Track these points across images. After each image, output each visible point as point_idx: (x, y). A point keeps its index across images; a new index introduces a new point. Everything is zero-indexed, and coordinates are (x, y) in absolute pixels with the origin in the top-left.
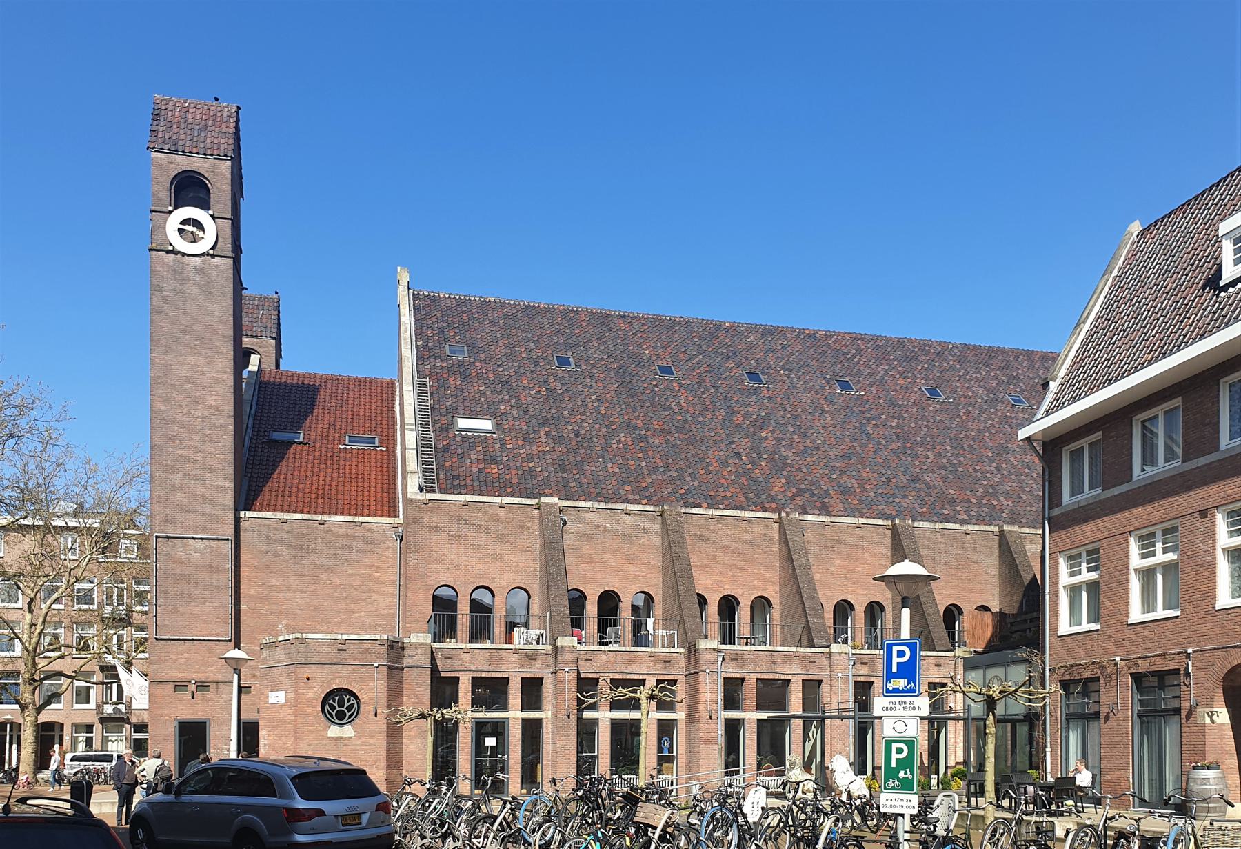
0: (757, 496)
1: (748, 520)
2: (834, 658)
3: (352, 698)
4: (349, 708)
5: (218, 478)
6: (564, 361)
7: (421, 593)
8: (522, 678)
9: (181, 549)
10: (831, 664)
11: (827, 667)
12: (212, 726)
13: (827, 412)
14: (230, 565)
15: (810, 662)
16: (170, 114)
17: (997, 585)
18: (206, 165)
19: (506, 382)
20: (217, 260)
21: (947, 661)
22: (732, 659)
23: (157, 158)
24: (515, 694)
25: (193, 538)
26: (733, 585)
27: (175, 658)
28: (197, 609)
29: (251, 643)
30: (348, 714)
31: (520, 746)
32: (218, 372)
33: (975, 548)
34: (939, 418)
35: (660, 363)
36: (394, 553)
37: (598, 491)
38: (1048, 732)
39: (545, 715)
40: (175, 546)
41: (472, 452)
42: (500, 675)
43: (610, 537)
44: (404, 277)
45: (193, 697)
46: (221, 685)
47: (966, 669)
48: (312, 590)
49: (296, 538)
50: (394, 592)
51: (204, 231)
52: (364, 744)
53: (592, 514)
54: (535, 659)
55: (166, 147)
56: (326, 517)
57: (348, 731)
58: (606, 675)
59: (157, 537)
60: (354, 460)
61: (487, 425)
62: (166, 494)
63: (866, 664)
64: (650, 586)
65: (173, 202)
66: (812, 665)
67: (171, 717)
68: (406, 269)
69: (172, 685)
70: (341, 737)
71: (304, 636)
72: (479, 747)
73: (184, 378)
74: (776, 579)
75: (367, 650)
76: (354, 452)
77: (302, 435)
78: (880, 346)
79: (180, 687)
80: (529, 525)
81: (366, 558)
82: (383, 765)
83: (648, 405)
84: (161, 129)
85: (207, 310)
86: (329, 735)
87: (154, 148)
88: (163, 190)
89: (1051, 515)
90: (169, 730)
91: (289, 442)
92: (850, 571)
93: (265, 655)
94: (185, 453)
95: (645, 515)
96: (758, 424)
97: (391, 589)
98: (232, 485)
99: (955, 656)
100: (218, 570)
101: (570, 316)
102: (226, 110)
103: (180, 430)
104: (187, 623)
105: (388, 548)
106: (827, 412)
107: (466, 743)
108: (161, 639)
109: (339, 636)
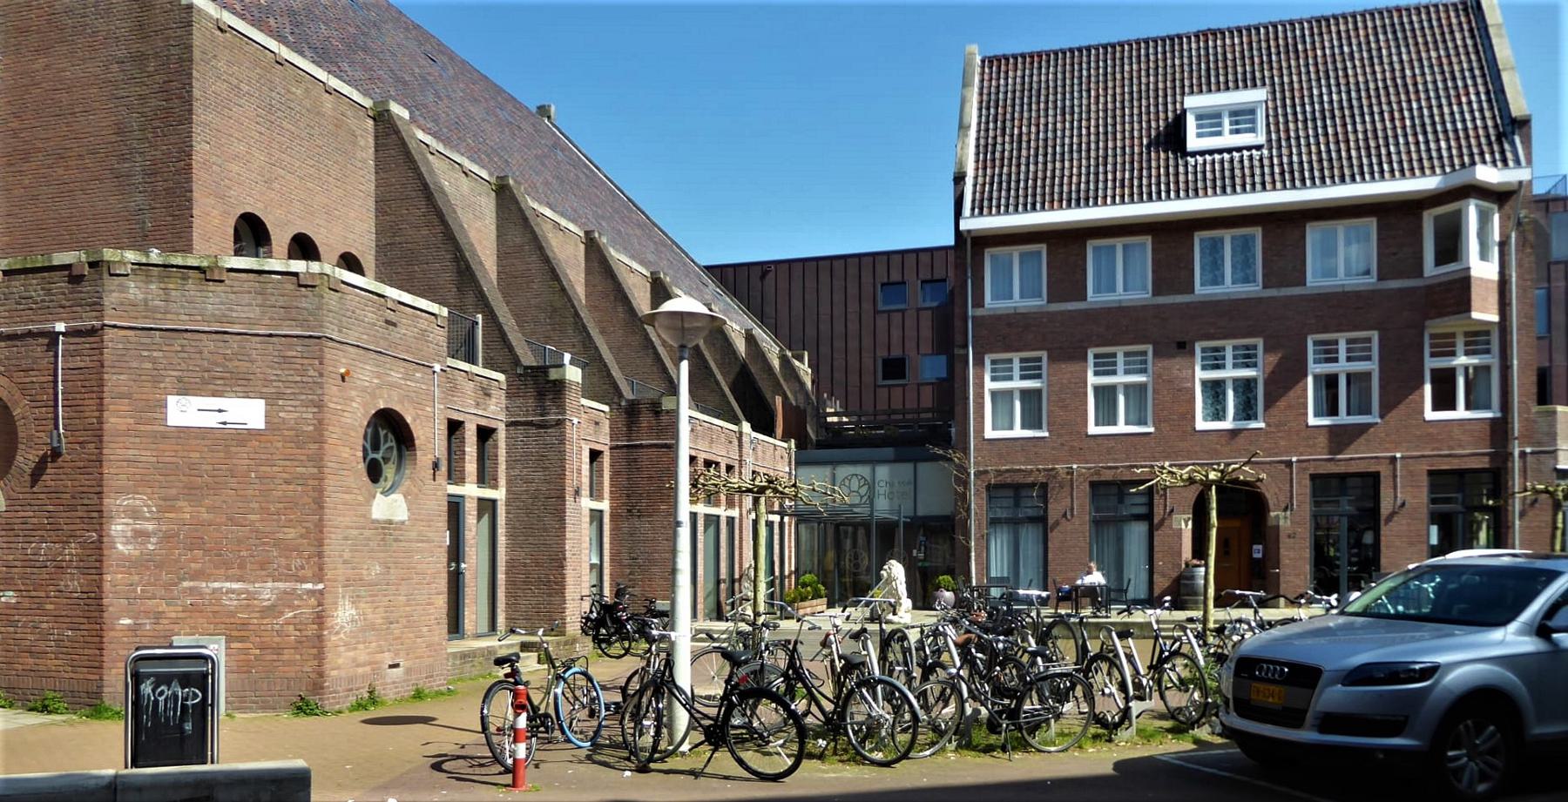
70: (390, 522)
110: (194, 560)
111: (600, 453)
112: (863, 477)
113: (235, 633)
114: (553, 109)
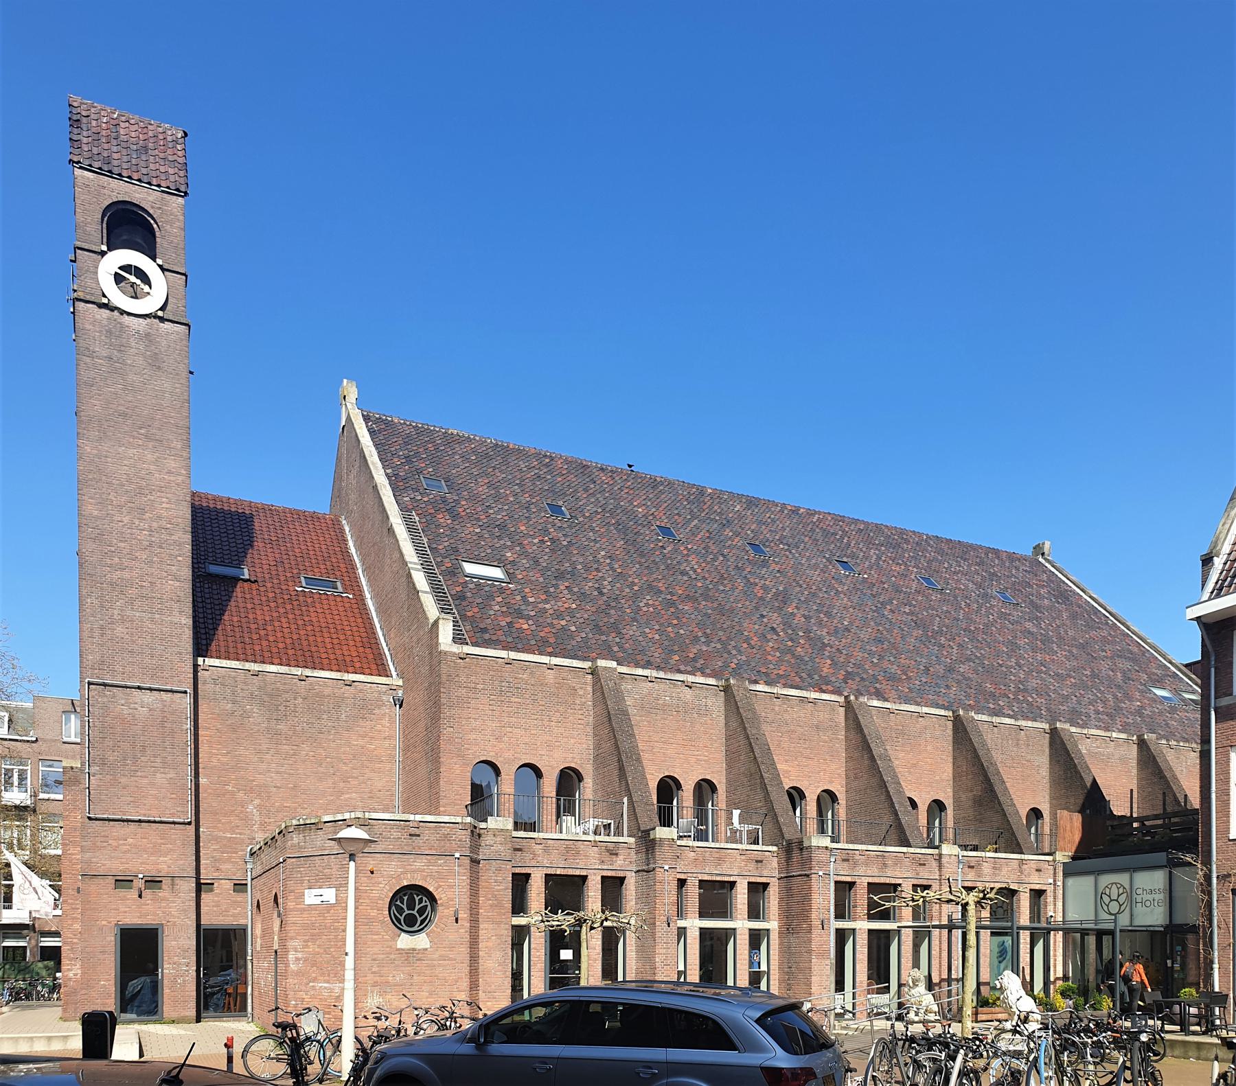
0: (810, 676)
1: (814, 702)
2: (944, 860)
3: (424, 898)
4: (421, 911)
5: (171, 609)
6: (556, 510)
7: (457, 769)
8: (602, 877)
9: (123, 702)
10: (940, 866)
11: (938, 872)
12: (166, 933)
13: (840, 593)
14: (189, 725)
15: (920, 864)
16: (94, 123)
17: (1048, 786)
18: (151, 199)
19: (503, 527)
20: (167, 325)
21: (1046, 866)
22: (844, 860)
23: (83, 177)
24: (741, 896)
25: (139, 688)
26: (799, 776)
27: (114, 843)
28: (146, 781)
29: (214, 827)
30: (419, 919)
31: (600, 959)
32: (169, 472)
33: (1028, 745)
34: (945, 608)
35: (658, 523)
36: (392, 722)
37: (646, 658)
38: (1216, 946)
39: (694, 924)
40: (114, 697)
41: (493, 603)
42: (577, 873)
43: (669, 713)
44: (352, 392)
45: (140, 896)
46: (177, 881)
47: (1066, 874)
48: (291, 762)
49: (271, 696)
50: (391, 769)
51: (151, 288)
52: (443, 958)
53: (651, 684)
54: (617, 854)
55: (97, 164)
56: (308, 672)
57: (421, 941)
58: (695, 875)
59: (89, 683)
60: (317, 605)
61: (497, 573)
62: (102, 628)
63: (973, 867)
64: (712, 772)
65: (105, 240)
66: (922, 868)
67: (110, 922)
68: (354, 383)
69: (111, 880)
70: (414, 950)
71: (367, 815)
72: (554, 962)
73: (125, 477)
74: (842, 771)
75: (446, 836)
76: (331, 598)
77: (246, 571)
78: (862, 530)
79: (123, 882)
80: (581, 693)
81: (358, 726)
82: (465, 984)
83: (663, 567)
84: (85, 140)
85: (156, 390)
86: (398, 947)
87: (78, 162)
88: (92, 227)
89: (1218, 705)
90: (108, 939)
91: (234, 578)
92: (914, 765)
93: (296, 840)
94: (126, 575)
95: (707, 689)
96: (780, 598)
97: (388, 766)
98: (190, 622)
99: (1054, 861)
100: (173, 731)
101: (547, 461)
102: (169, 133)
103: (119, 544)
104: (132, 799)
105: (384, 715)
106: (840, 593)
107: (538, 957)
108: (96, 819)
109: (411, 817)
110: (313, 972)
111: (765, 886)
112: (1122, 885)
113: (327, 1010)
114: (1047, 545)
